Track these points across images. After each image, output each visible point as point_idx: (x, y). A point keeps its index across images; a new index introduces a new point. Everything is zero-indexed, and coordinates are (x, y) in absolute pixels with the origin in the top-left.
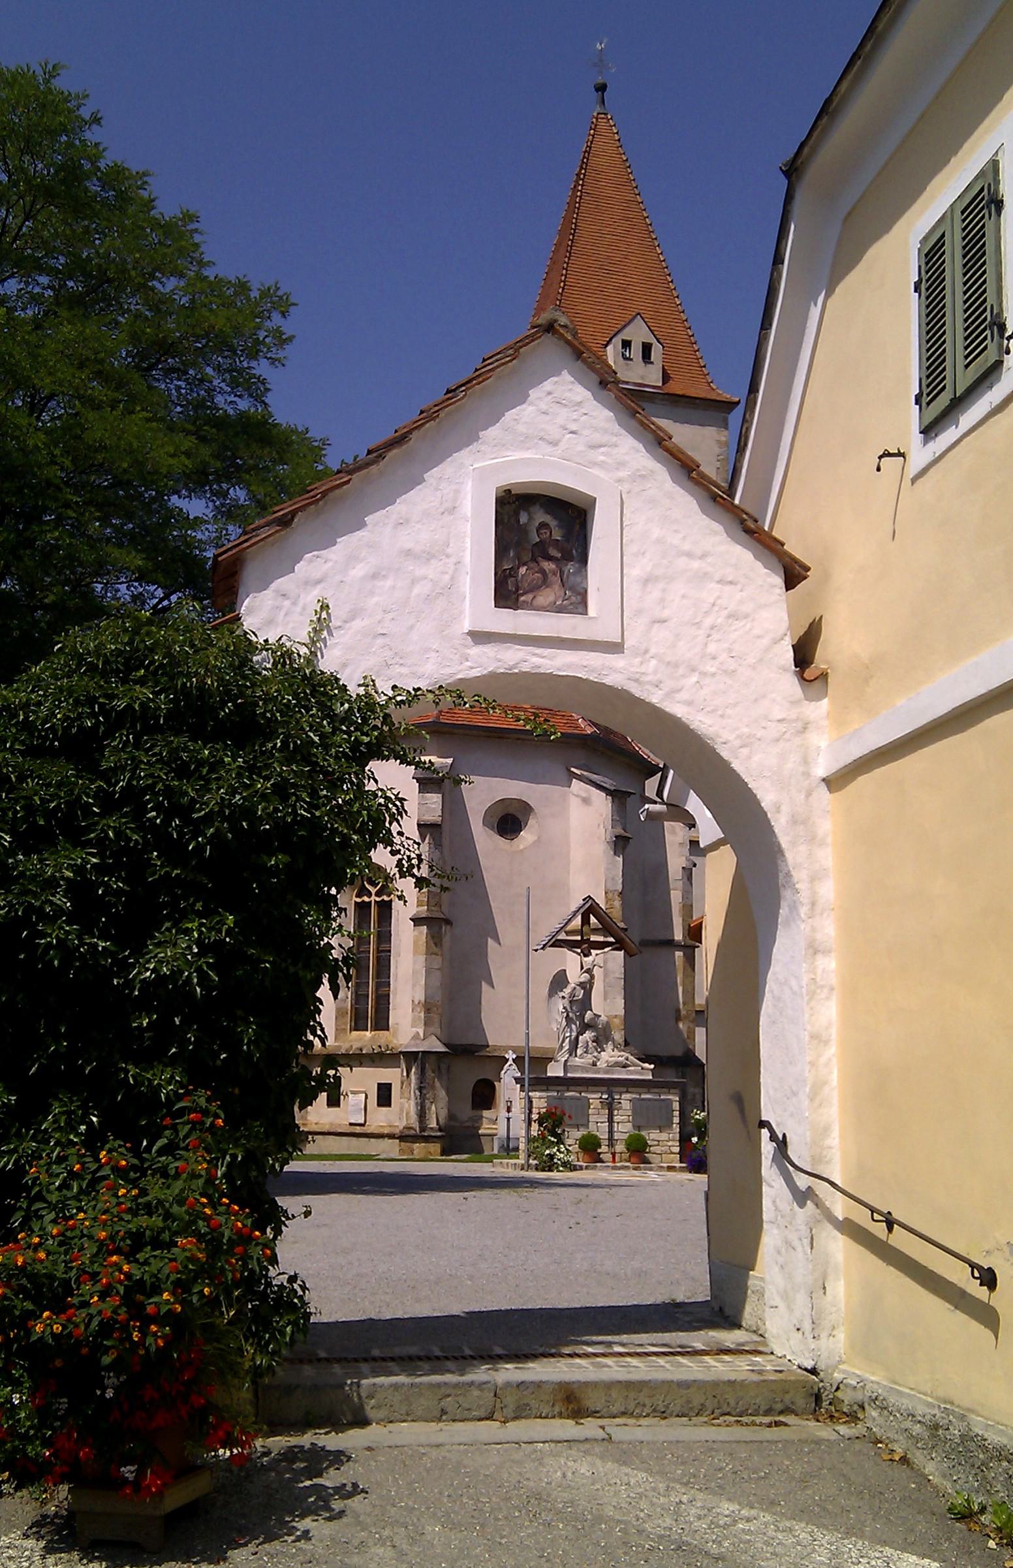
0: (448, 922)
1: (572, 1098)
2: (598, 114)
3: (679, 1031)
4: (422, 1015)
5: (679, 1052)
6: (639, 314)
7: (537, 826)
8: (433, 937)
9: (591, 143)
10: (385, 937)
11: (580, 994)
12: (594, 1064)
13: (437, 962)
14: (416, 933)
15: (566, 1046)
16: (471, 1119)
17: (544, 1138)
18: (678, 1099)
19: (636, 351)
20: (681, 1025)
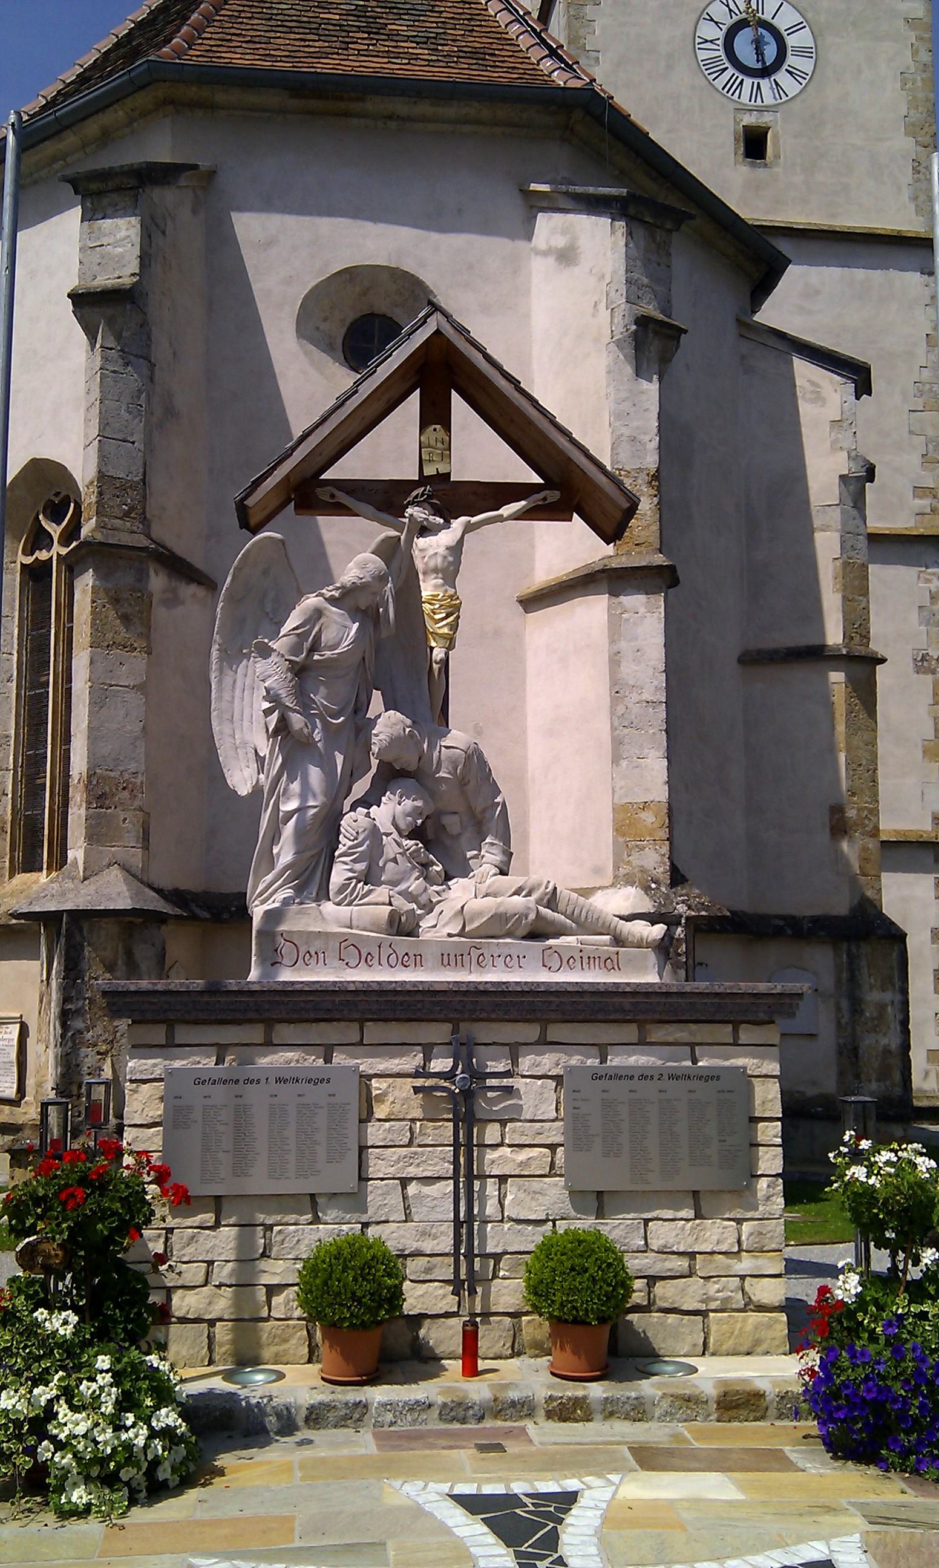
3: (839, 858)
5: (840, 906)
8: (116, 601)
18: (774, 1068)
20: (845, 846)
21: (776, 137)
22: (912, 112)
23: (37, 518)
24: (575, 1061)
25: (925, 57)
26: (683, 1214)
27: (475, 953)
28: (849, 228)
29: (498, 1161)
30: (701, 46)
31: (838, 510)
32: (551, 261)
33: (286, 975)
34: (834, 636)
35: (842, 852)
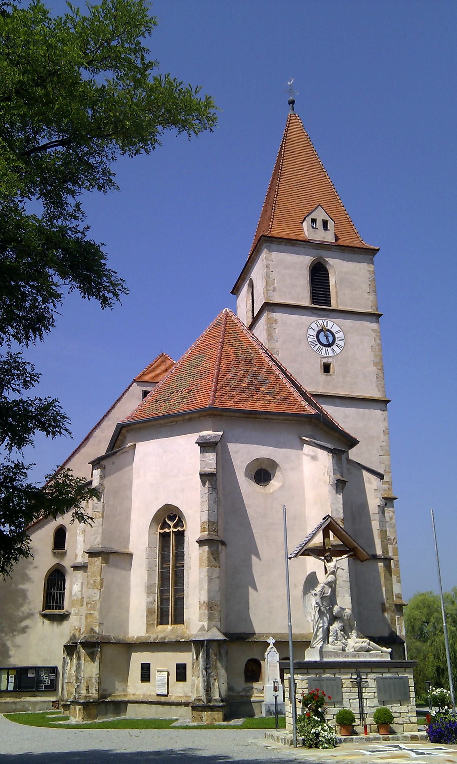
0: (223, 543)
1: (328, 679)
2: (291, 114)
3: (385, 619)
4: (206, 612)
5: (386, 634)
6: (320, 205)
7: (281, 476)
8: (212, 554)
9: (288, 127)
10: (180, 556)
11: (329, 591)
12: (344, 650)
13: (216, 572)
14: (201, 551)
15: (320, 635)
16: (245, 690)
17: (309, 718)
18: (412, 676)
19: (319, 224)
20: (386, 615)
21: (333, 366)
22: (375, 359)
23: (165, 519)
24: (377, 676)
25: (378, 341)
26: (398, 705)
27: (358, 655)
28: (357, 396)
29: (365, 695)
30: (310, 337)
31: (378, 515)
32: (309, 458)
33: (325, 660)
34: (379, 552)
35: (385, 617)
